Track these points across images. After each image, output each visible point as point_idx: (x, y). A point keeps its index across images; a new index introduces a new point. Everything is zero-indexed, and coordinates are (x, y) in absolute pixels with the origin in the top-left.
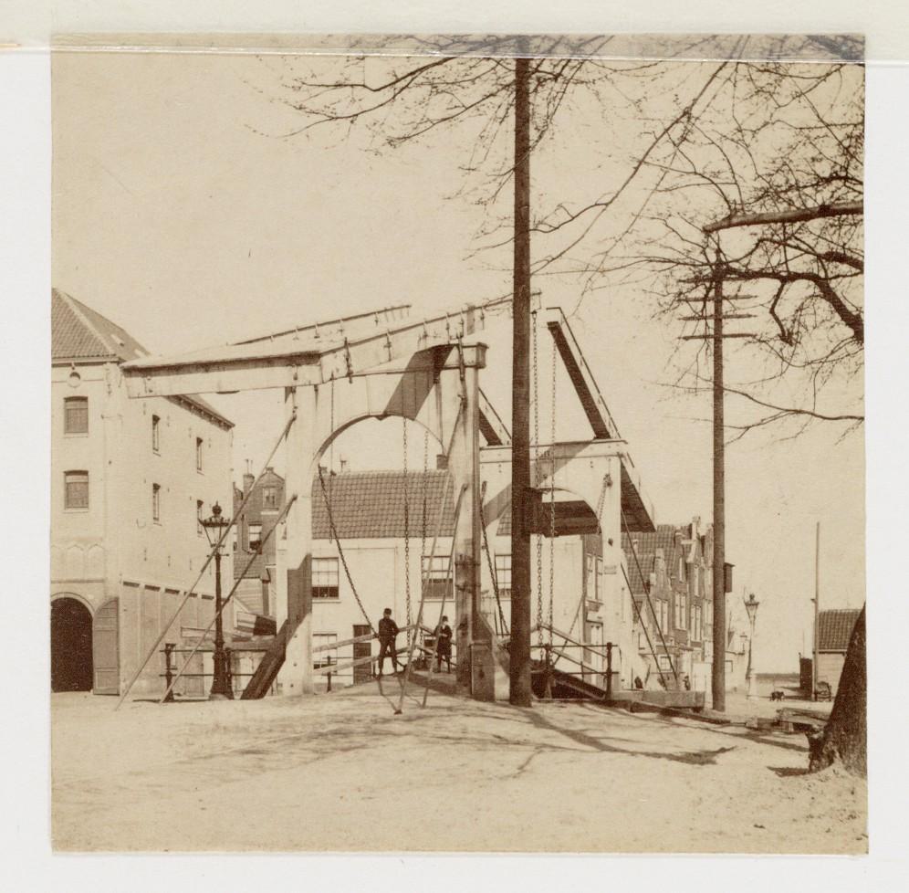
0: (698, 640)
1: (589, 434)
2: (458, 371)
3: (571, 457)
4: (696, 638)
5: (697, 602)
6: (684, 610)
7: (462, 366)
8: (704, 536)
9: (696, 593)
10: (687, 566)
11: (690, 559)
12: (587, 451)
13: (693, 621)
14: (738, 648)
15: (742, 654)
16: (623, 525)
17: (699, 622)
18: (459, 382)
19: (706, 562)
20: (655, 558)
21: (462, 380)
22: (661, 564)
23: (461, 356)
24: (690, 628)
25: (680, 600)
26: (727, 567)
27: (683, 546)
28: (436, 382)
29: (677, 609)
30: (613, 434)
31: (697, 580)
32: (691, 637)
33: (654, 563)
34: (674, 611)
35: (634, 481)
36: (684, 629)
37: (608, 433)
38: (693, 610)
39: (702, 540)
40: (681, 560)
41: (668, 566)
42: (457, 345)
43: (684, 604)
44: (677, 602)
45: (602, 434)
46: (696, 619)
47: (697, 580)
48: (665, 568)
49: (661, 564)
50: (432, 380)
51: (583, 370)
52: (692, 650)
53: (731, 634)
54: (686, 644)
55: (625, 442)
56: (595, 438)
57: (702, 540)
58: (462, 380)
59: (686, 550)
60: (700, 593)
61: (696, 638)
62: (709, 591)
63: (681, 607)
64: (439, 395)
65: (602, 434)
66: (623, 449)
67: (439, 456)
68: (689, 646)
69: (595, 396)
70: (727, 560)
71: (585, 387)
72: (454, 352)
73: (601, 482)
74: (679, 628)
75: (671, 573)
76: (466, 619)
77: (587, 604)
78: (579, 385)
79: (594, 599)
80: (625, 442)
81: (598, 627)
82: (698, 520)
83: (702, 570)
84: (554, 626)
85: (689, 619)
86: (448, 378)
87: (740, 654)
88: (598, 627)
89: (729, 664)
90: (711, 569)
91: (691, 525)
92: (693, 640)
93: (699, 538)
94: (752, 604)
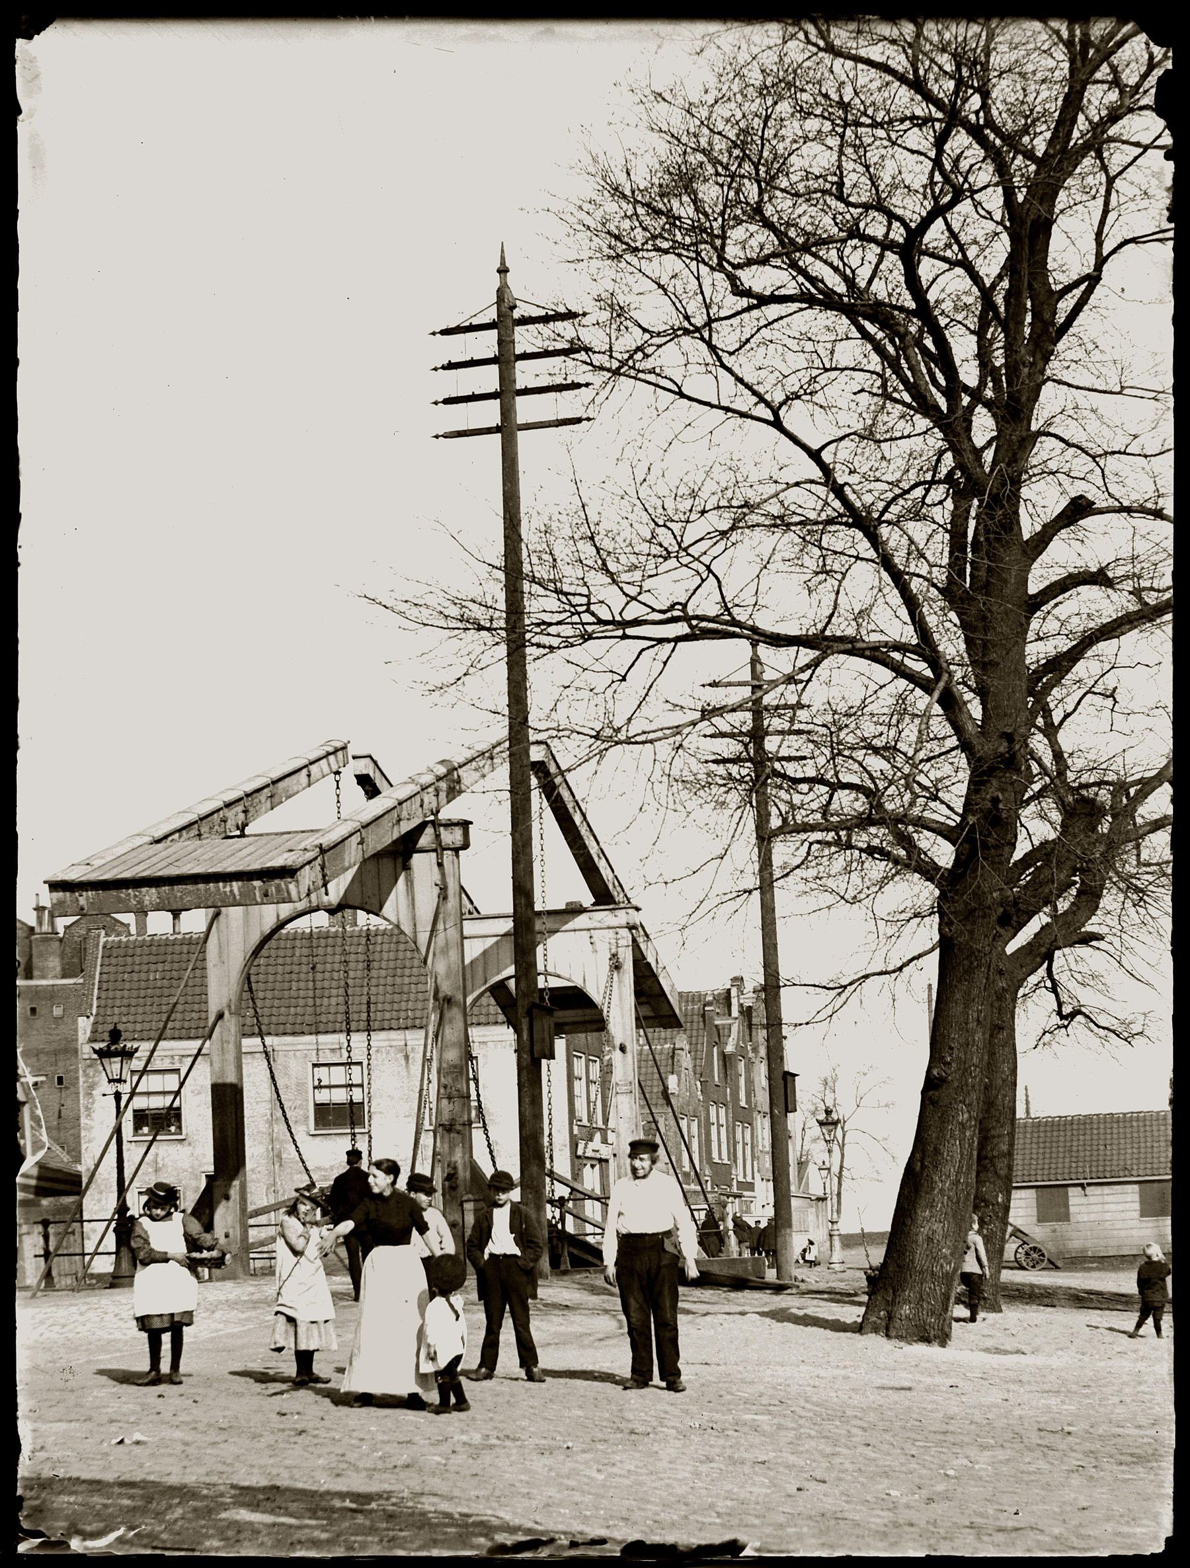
0: (749, 1179)
1: (587, 899)
2: (434, 855)
3: (557, 931)
4: (745, 1177)
5: (743, 1116)
6: (723, 1131)
7: (439, 848)
8: (750, 1007)
9: (743, 1104)
10: (725, 1059)
11: (730, 1048)
12: (581, 921)
13: (740, 1147)
14: (816, 1190)
15: (823, 1199)
16: (637, 1019)
17: (748, 1148)
18: (436, 868)
19: (755, 1050)
20: (674, 1049)
21: (440, 865)
22: (685, 1060)
23: (438, 836)
24: (735, 1161)
25: (720, 1115)
26: (788, 1077)
27: (716, 1026)
28: (407, 867)
29: (714, 1129)
30: (619, 897)
31: (742, 1081)
32: (738, 1174)
33: (673, 1057)
34: (708, 1134)
35: (651, 959)
36: (726, 1162)
37: (612, 897)
38: (739, 1130)
39: (747, 1012)
40: (715, 1049)
41: (695, 1059)
42: (432, 822)
43: (723, 1121)
44: (713, 1119)
45: (604, 896)
46: (745, 1144)
47: (742, 1081)
48: (690, 1067)
49: (685, 1060)
50: (399, 865)
51: (602, 864)
52: (740, 1196)
53: (802, 1165)
54: (730, 1186)
55: (638, 909)
56: (593, 905)
57: (747, 1012)
58: (440, 865)
59: (719, 1035)
60: (748, 1101)
61: (745, 1177)
62: (762, 1098)
63: (719, 1126)
64: (410, 883)
65: (604, 896)
66: (635, 917)
67: (554, 1058)
68: (735, 1190)
69: (593, 849)
70: (789, 1067)
71: (580, 837)
72: (429, 831)
73: (606, 965)
74: (717, 1160)
75: (702, 1075)
76: (455, 1168)
77: (576, 1130)
78: (579, 849)
79: (585, 1122)
80: (638, 909)
81: (593, 1166)
82: (738, 981)
83: (750, 1065)
84: (555, 1170)
85: (732, 1143)
86: (422, 863)
87: (819, 1199)
88: (593, 1166)
89: (1131, 1327)
90: (765, 1062)
91: (729, 990)
92: (741, 1179)
93: (741, 1012)
94: (829, 1122)
